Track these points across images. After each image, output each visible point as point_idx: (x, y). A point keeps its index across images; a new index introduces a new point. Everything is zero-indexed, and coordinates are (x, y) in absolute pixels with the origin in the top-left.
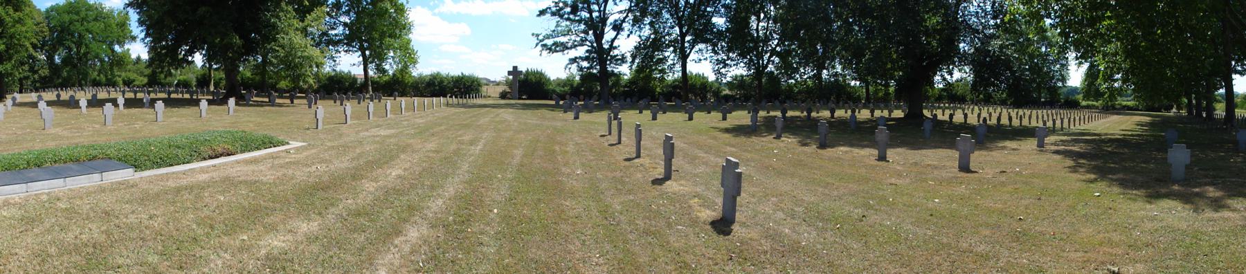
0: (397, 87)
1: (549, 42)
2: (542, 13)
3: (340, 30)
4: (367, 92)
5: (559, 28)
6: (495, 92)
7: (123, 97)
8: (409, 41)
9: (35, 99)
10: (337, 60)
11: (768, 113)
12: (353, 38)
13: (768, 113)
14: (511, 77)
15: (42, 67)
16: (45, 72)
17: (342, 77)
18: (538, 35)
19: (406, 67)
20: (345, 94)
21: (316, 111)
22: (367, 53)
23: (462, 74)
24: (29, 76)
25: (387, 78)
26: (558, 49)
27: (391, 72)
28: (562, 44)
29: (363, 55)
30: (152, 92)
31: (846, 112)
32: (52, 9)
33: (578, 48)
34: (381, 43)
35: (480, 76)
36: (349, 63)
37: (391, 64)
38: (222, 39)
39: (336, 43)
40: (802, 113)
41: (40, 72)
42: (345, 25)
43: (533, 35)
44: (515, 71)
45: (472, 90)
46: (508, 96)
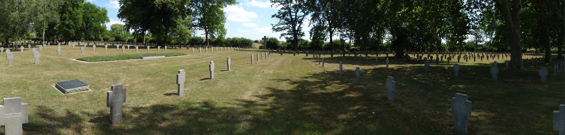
0: (219, 43)
1: (276, 27)
2: (273, 16)
3: (197, 21)
4: (207, 45)
5: (281, 22)
6: (257, 46)
8: (223, 26)
10: (196, 32)
11: (349, 55)
12: (202, 24)
13: (349, 55)
14: (263, 40)
17: (197, 39)
18: (273, 25)
19: (222, 35)
20: (199, 45)
22: (207, 30)
25: (215, 39)
26: (279, 30)
27: (216, 37)
28: (280, 28)
29: (206, 31)
31: (414, 56)
33: (286, 30)
34: (213, 26)
36: (200, 33)
37: (216, 34)
38: (159, 27)
39: (196, 26)
40: (341, 55)
42: (199, 19)
43: (271, 24)
44: (265, 38)
45: (248, 45)
46: (263, 48)
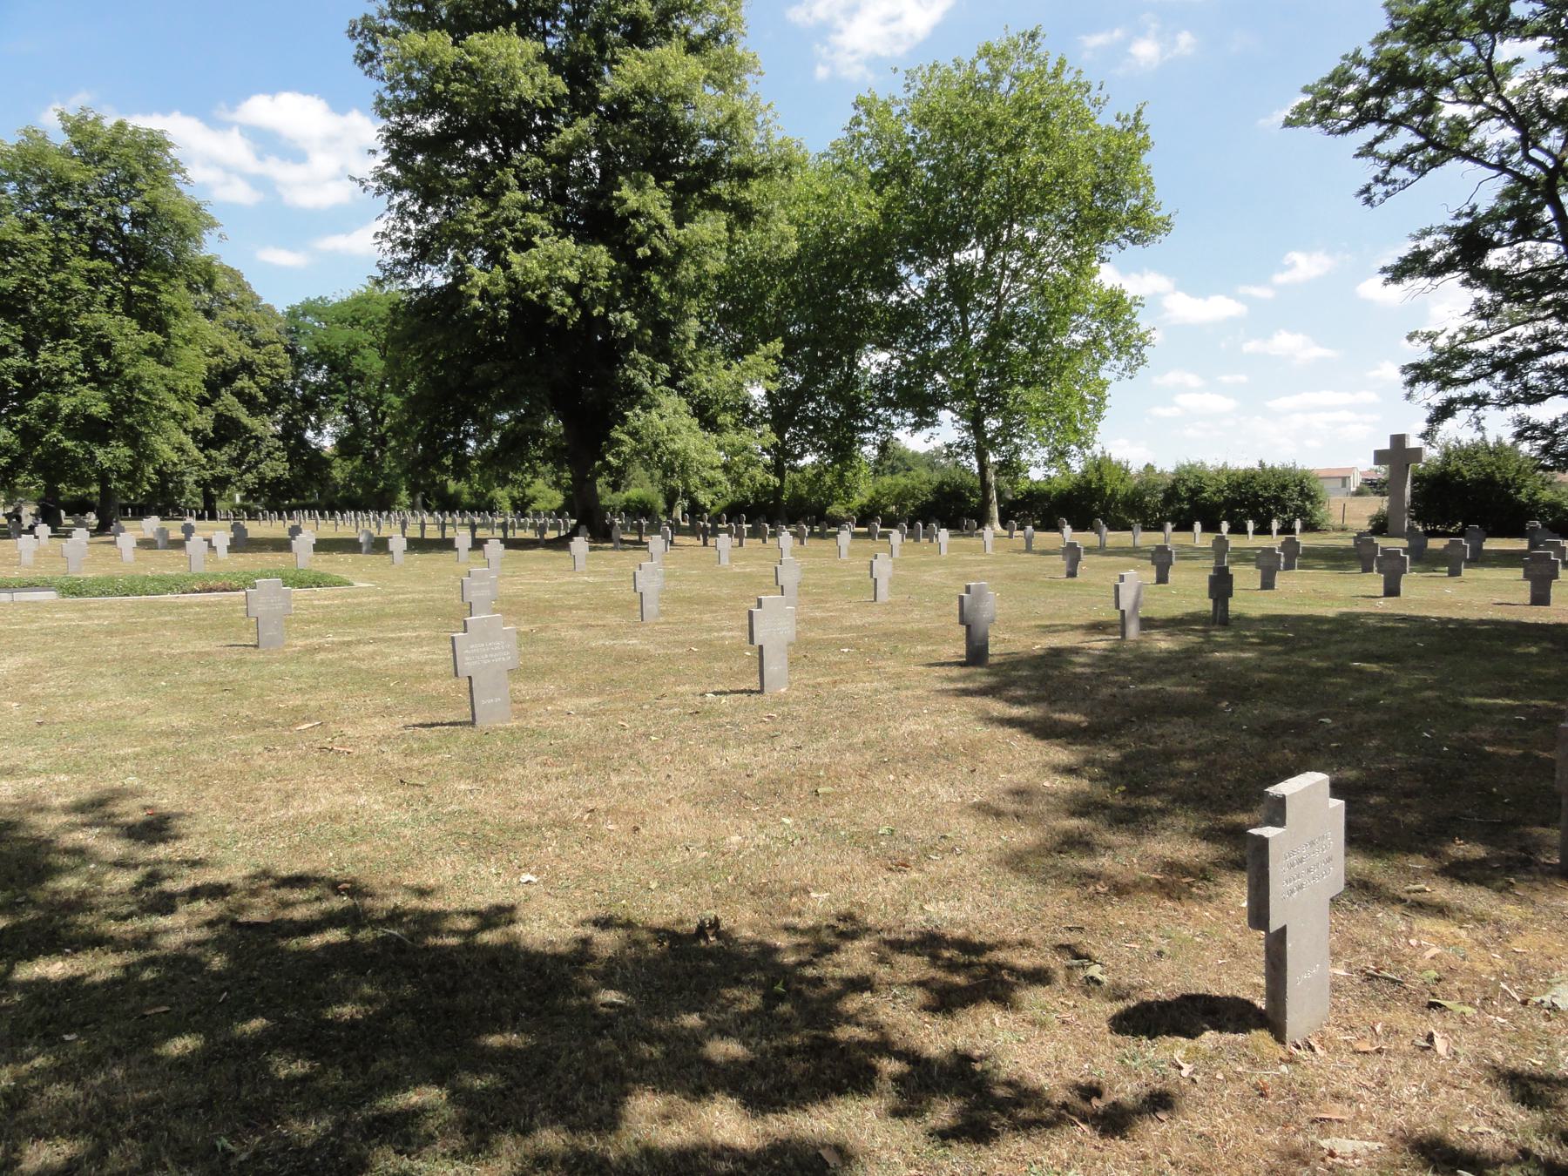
7: (403, 533)
9: (284, 534)
15: (269, 454)
16: (277, 467)
21: (1117, 588)
23: (1262, 464)
24: (229, 477)
30: (482, 526)
32: (309, 308)
35: (1309, 466)
41: (262, 466)
